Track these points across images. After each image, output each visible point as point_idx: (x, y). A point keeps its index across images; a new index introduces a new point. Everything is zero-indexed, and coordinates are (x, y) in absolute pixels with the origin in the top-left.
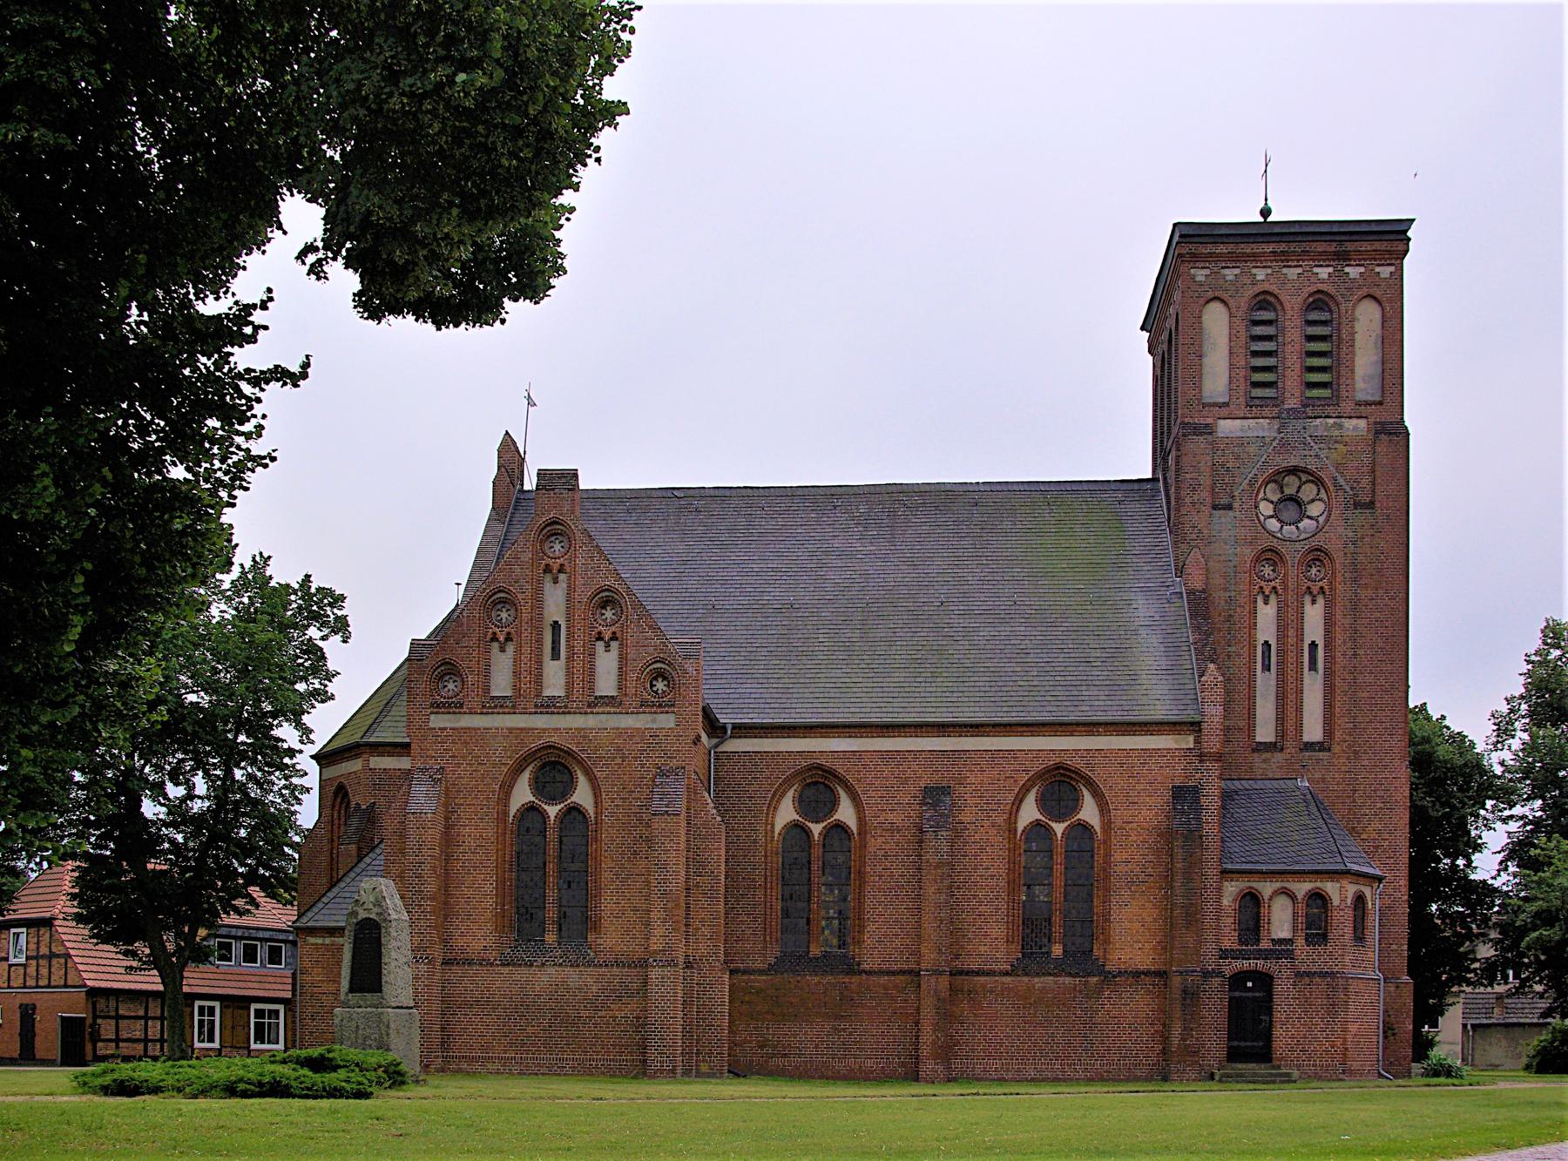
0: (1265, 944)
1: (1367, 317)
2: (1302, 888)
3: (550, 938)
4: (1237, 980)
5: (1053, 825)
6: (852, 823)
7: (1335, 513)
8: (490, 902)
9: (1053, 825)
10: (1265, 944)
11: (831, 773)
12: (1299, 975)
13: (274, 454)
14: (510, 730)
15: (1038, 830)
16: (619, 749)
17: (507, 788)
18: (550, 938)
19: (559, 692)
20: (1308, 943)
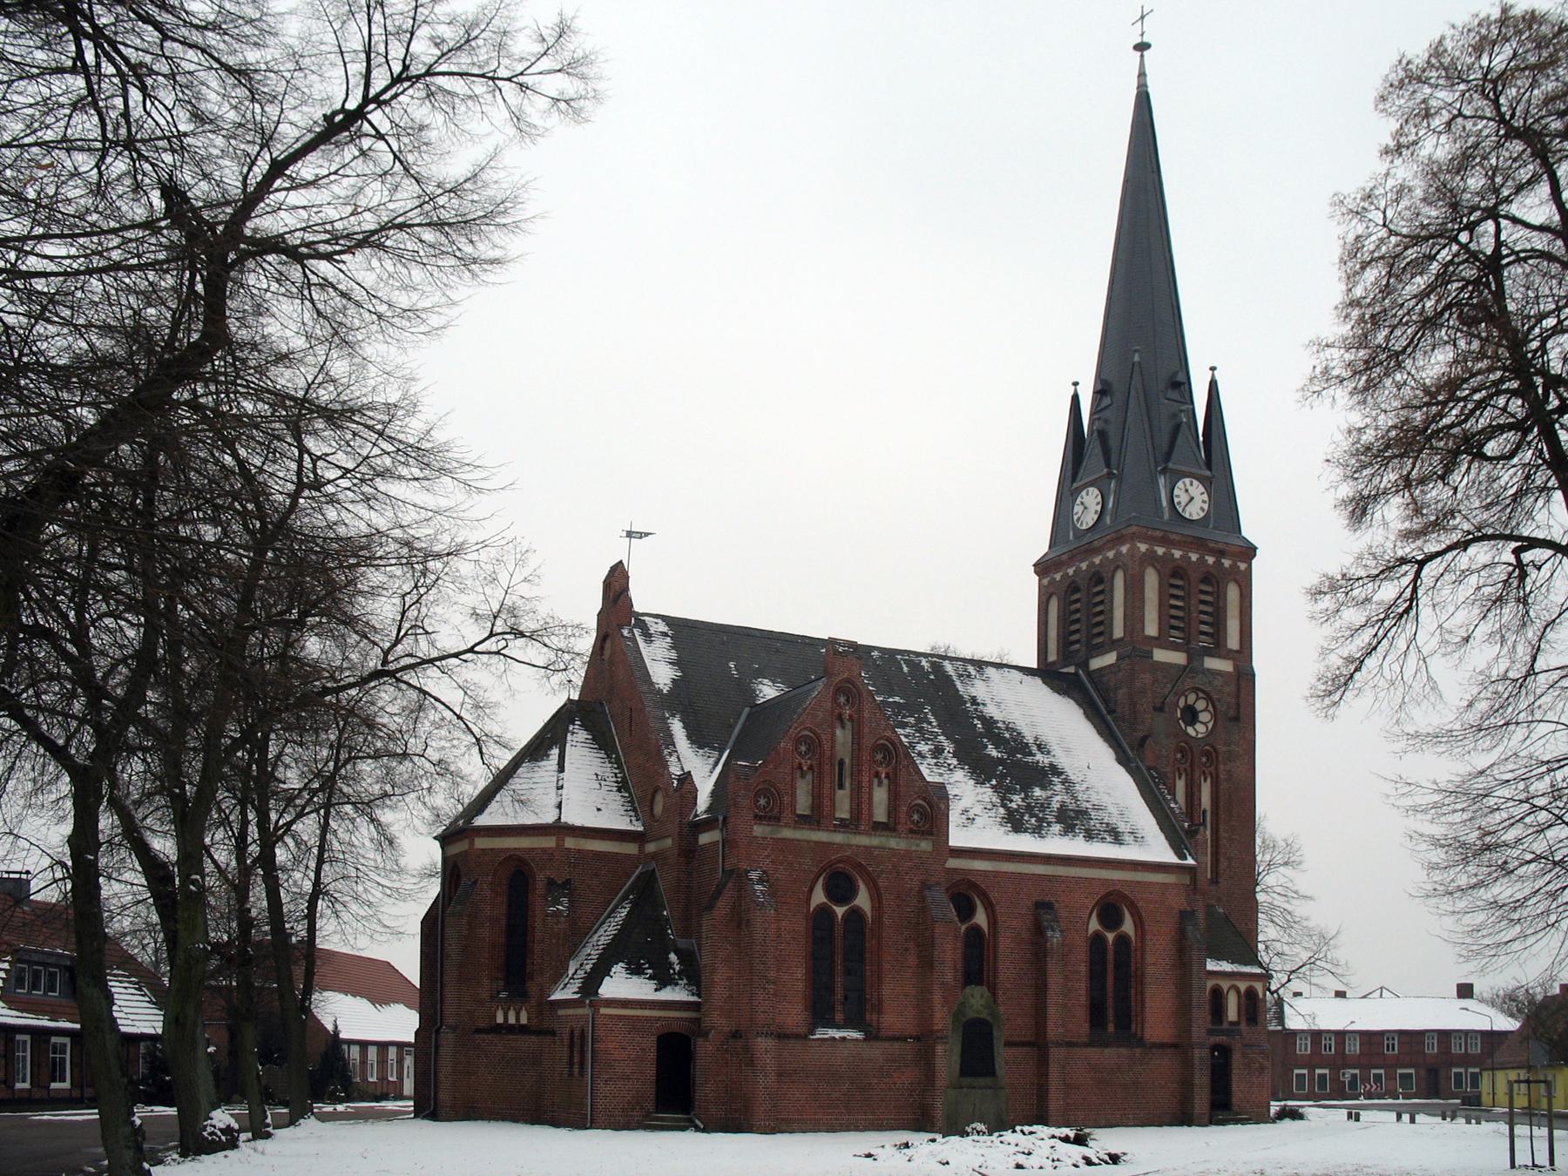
0: (1225, 1026)
1: (1232, 593)
2: (1243, 986)
3: (1111, 1028)
4: (1214, 1047)
5: (844, 909)
6: (984, 926)
7: (1219, 723)
8: (801, 986)
9: (844, 909)
10: (1225, 1026)
11: (973, 886)
12: (1245, 1045)
13: (537, 572)
14: (816, 843)
15: (823, 911)
16: (894, 866)
17: (1139, 924)
18: (1111, 1028)
19: (846, 815)
20: (1248, 1025)
